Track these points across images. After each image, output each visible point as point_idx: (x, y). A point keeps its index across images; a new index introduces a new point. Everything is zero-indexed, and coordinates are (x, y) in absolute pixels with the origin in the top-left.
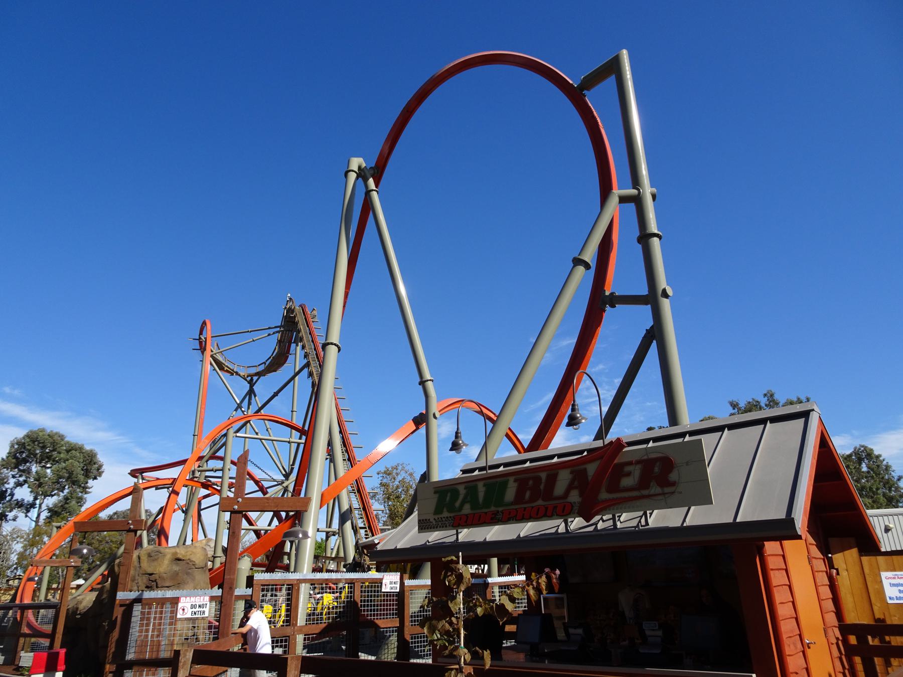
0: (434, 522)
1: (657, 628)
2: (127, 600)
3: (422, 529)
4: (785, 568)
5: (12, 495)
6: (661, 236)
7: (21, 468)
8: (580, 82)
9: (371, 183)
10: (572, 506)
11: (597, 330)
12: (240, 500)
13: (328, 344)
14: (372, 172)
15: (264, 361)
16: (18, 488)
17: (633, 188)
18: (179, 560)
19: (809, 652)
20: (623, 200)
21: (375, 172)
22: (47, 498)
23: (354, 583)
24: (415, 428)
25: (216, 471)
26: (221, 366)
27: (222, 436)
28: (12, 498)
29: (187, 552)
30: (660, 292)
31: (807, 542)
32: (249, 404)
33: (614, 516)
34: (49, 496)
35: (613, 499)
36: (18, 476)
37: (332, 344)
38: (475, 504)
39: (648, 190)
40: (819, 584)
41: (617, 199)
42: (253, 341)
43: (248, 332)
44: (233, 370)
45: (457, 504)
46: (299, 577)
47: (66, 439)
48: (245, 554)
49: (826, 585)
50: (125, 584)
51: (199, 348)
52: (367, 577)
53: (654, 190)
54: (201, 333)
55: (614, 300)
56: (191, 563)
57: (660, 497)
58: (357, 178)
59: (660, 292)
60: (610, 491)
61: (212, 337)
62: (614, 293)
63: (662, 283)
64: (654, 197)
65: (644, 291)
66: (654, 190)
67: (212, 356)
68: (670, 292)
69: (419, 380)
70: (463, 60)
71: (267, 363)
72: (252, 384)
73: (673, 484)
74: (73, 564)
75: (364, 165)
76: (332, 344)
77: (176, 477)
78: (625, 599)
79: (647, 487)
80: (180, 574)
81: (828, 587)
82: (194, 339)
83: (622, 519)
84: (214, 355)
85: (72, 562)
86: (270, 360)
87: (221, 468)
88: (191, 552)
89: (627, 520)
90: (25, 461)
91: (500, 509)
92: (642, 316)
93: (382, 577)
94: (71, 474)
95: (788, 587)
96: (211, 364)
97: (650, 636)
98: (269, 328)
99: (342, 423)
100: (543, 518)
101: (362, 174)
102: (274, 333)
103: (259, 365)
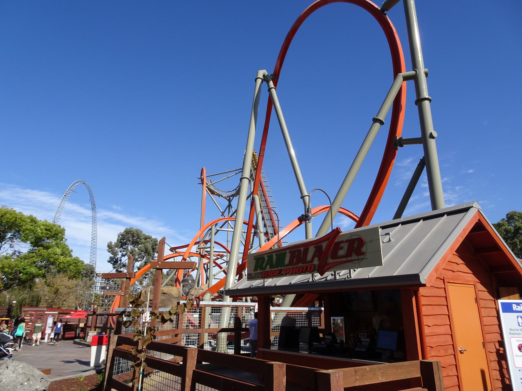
0: (254, 275)
1: (366, 337)
2: (119, 311)
3: (249, 279)
4: (447, 304)
5: (121, 260)
6: (430, 99)
7: (124, 247)
8: (382, 7)
9: (271, 84)
10: (315, 267)
11: (392, 161)
12: (160, 263)
13: (243, 178)
14: (272, 77)
15: (236, 188)
16: (123, 257)
17: (413, 70)
18: (165, 293)
20: (405, 78)
21: (273, 77)
22: (137, 262)
23: (238, 308)
24: (299, 223)
25: (207, 248)
26: (213, 192)
27: (209, 230)
28: (121, 262)
29: (169, 290)
30: (428, 135)
31: (476, 290)
32: (229, 212)
33: (335, 272)
34: (137, 261)
35: (336, 262)
36: (122, 251)
37: (245, 178)
39: (422, 69)
40: (483, 315)
41: (402, 79)
42: (228, 177)
43: (225, 173)
44: (219, 194)
45: (264, 265)
46: (205, 303)
47: (143, 233)
48: (208, 292)
49: (495, 316)
50: (126, 304)
51: (201, 183)
52: (246, 305)
53: (427, 70)
54: (202, 175)
55: (402, 142)
56: (171, 295)
57: (357, 261)
58: (262, 82)
59: (428, 135)
60: (332, 258)
61: (206, 177)
62: (402, 138)
63: (431, 129)
64: (426, 74)
65: (419, 135)
66: (427, 70)
67: (207, 187)
68: (435, 134)
69: (300, 196)
70: (312, 5)
71: (237, 189)
72: (230, 201)
73: (363, 254)
74: (123, 294)
75: (267, 74)
76: (245, 178)
77: (185, 252)
79: (350, 255)
80: (165, 301)
81: (496, 318)
82: (198, 178)
83: (341, 274)
84: (208, 186)
85: (122, 294)
86: (238, 187)
87: (209, 247)
88: (170, 290)
89: (342, 274)
90: (125, 244)
91: (283, 268)
93: (255, 305)
94: (147, 249)
95: (447, 316)
96: (206, 190)
97: (327, 339)
98: (236, 170)
99: (274, 221)
100: (302, 273)
101: (265, 79)
102: (238, 173)
103: (233, 191)
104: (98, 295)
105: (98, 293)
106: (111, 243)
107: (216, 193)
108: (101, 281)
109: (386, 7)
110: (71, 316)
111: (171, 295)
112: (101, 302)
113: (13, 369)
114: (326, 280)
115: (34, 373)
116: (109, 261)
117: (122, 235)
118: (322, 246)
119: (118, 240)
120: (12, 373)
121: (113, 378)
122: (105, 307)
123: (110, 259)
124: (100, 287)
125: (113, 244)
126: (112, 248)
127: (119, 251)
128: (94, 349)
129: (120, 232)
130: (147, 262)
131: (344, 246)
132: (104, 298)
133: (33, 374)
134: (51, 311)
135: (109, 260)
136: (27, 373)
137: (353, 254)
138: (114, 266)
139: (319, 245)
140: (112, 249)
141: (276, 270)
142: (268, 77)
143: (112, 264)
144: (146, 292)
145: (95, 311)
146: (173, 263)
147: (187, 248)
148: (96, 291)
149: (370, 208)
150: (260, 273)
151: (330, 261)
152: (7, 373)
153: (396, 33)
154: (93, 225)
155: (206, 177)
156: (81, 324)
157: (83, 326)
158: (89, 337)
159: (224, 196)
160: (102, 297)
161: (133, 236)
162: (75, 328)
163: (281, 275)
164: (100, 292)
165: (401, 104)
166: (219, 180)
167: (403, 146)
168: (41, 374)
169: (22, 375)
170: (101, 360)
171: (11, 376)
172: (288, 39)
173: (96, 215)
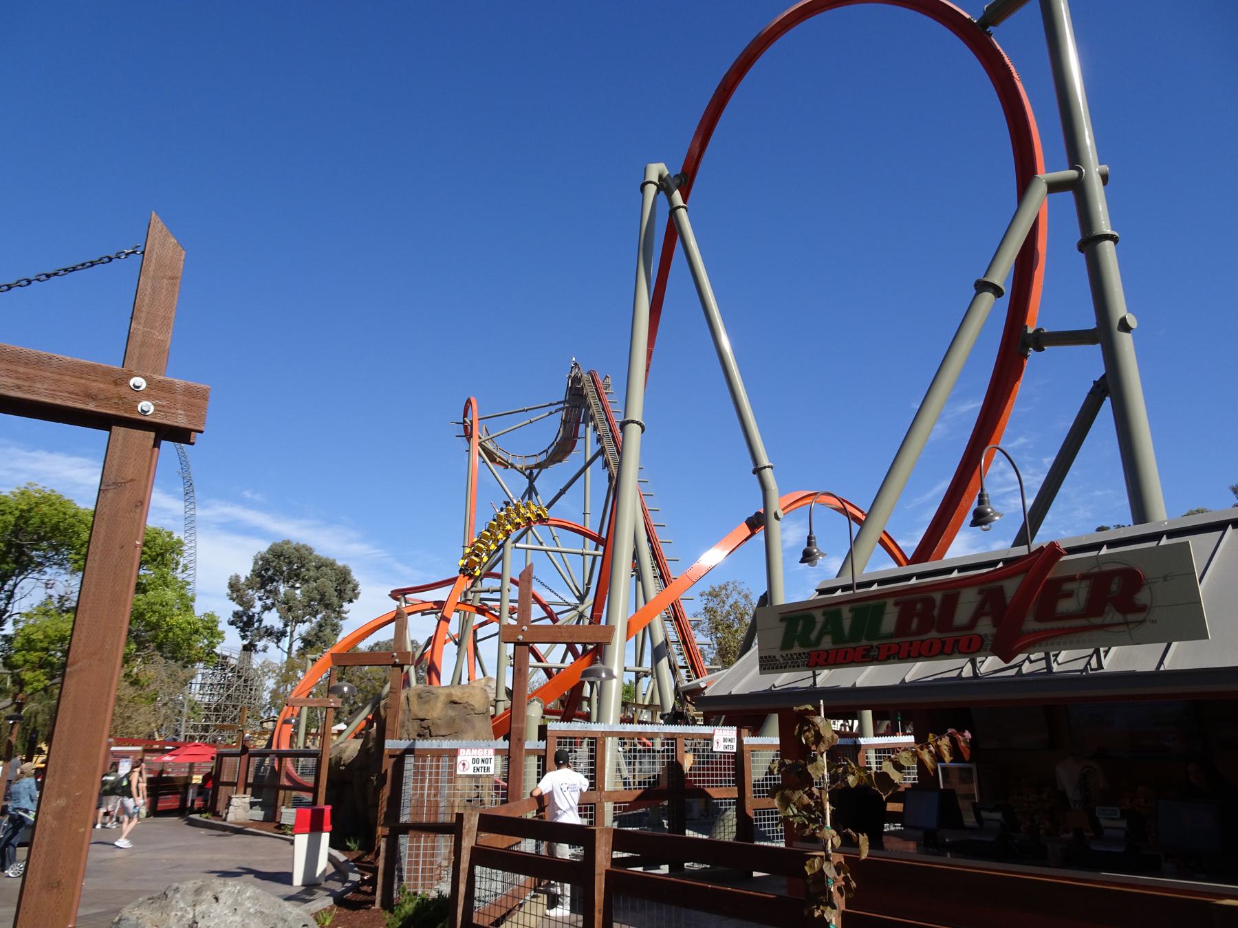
0: (781, 659)
1: (1119, 816)
3: (764, 669)
5: (260, 621)
6: (1117, 237)
7: (268, 588)
9: (677, 196)
11: (1016, 385)
12: (525, 628)
13: (628, 422)
14: (678, 181)
16: (266, 612)
17: (1071, 169)
20: (1053, 187)
21: (681, 181)
22: (299, 624)
23: (676, 739)
25: (493, 591)
26: (492, 457)
28: (260, 624)
30: (1116, 323)
33: (1047, 654)
34: (301, 622)
37: (633, 422)
39: (1094, 168)
42: (531, 422)
43: (524, 410)
44: (507, 462)
45: (813, 636)
47: (315, 553)
48: (535, 698)
53: (1105, 168)
54: (465, 415)
55: (1041, 340)
56: (469, 707)
58: (658, 192)
59: (1116, 323)
60: (1039, 618)
61: (479, 419)
62: (1041, 329)
63: (1120, 308)
64: (1105, 178)
65: (1089, 322)
66: (1105, 168)
67: (480, 444)
68: (1132, 322)
69: (752, 467)
70: (800, 5)
72: (531, 478)
74: (332, 704)
75: (666, 173)
76: (633, 422)
79: (1100, 613)
80: (457, 721)
82: (457, 423)
83: (1060, 659)
84: (483, 443)
90: (272, 580)
91: (875, 643)
93: (712, 732)
94: (323, 595)
96: (480, 455)
97: (987, 820)
98: (551, 405)
99: (651, 528)
101: (664, 186)
102: (556, 411)
103: (539, 454)
104: (196, 704)
105: (196, 699)
106: (237, 577)
107: (498, 459)
108: (205, 671)
109: (994, 16)
110: (174, 757)
111: (469, 707)
112: (204, 720)
113: (230, 902)
114: (1019, 673)
115: (285, 911)
116: (232, 621)
117: (262, 558)
118: (1001, 589)
119: (253, 571)
120: (230, 914)
121: (475, 921)
122: (212, 733)
123: (234, 617)
124: (201, 684)
125: (243, 580)
126: (238, 591)
127: (257, 598)
128: (302, 841)
129: (259, 553)
130: (324, 625)
131: (1076, 591)
132: (210, 711)
133: (283, 915)
134: (127, 744)
135: (232, 619)
136: (266, 911)
137: (1106, 610)
138: (242, 634)
139: (992, 585)
140: (238, 593)
141: (855, 648)
142: (670, 181)
143: (239, 629)
144: (408, 699)
145: (246, 745)
146: (558, 630)
147: (450, 587)
148: (191, 695)
149: (961, 498)
150: (800, 654)
151: (1031, 625)
152: (218, 912)
153: (1019, 79)
154: (187, 535)
155: (479, 419)
156: (195, 777)
157: (200, 782)
158: (234, 810)
159: (518, 467)
160: (206, 708)
161: (290, 563)
162: (181, 786)
163: (871, 659)
164: (201, 696)
165: (1037, 250)
166: (520, 425)
167: (1044, 349)
168: (301, 915)
169: (255, 917)
170: (319, 871)
171: (229, 921)
172: (724, 90)
173: (194, 508)
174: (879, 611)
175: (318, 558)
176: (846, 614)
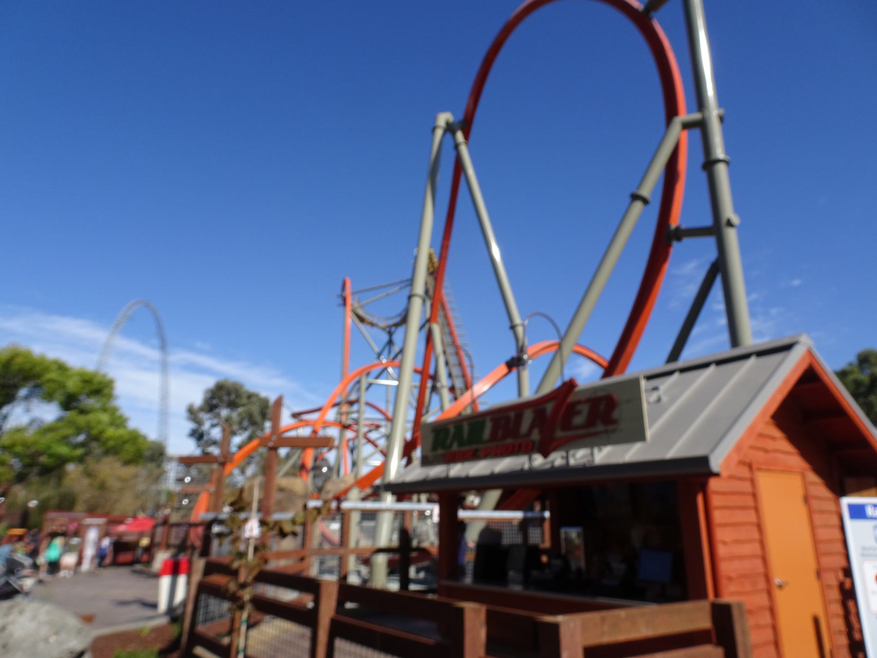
9: (460, 136)
19: (779, 595)
20: (686, 126)
26: (362, 320)
38: (461, 444)
39: (714, 111)
45: (448, 441)
55: (679, 234)
63: (728, 211)
64: (721, 119)
68: (735, 220)
72: (390, 334)
78: (636, 535)
89: (579, 456)
92: (707, 248)
101: (450, 129)
174: (482, 425)
175: (247, 392)
176: (466, 428)
